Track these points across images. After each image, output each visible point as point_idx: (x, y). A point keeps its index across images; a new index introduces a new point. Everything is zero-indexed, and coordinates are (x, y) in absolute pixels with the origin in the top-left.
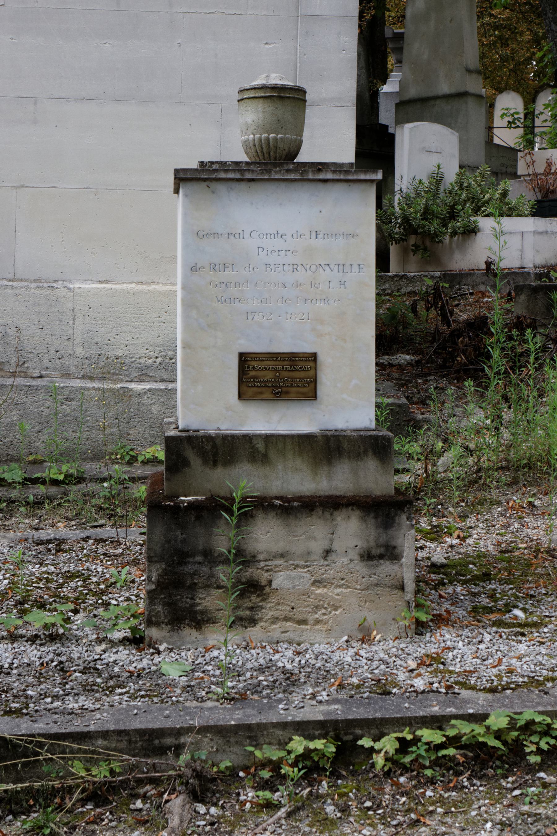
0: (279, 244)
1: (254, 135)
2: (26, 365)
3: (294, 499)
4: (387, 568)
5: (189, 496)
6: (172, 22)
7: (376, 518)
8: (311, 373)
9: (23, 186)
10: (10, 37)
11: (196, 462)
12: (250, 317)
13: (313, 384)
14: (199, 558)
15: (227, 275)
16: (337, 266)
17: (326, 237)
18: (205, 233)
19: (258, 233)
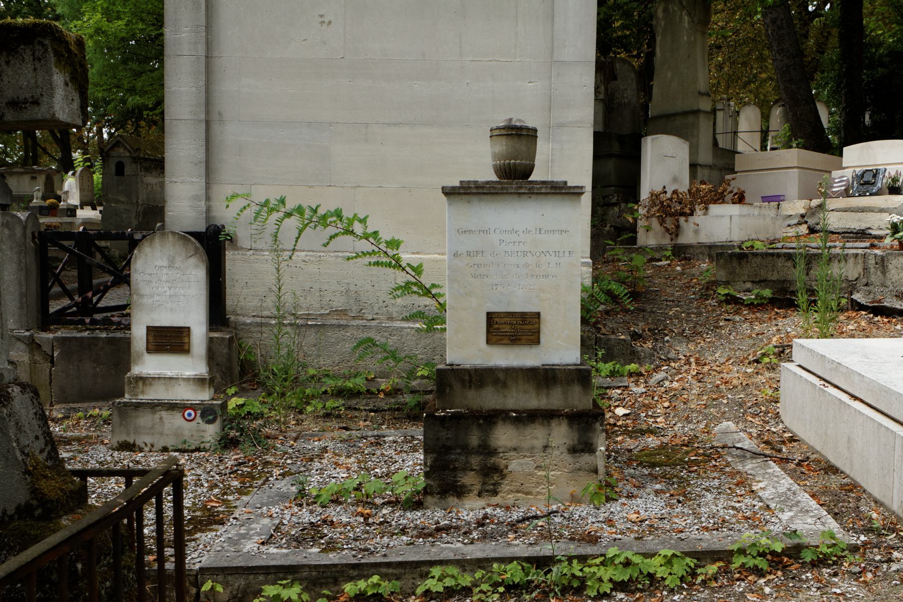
3: (524, 412)
4: (586, 458)
7: (579, 424)
8: (536, 326)
11: (457, 386)
14: (458, 451)
15: (478, 259)
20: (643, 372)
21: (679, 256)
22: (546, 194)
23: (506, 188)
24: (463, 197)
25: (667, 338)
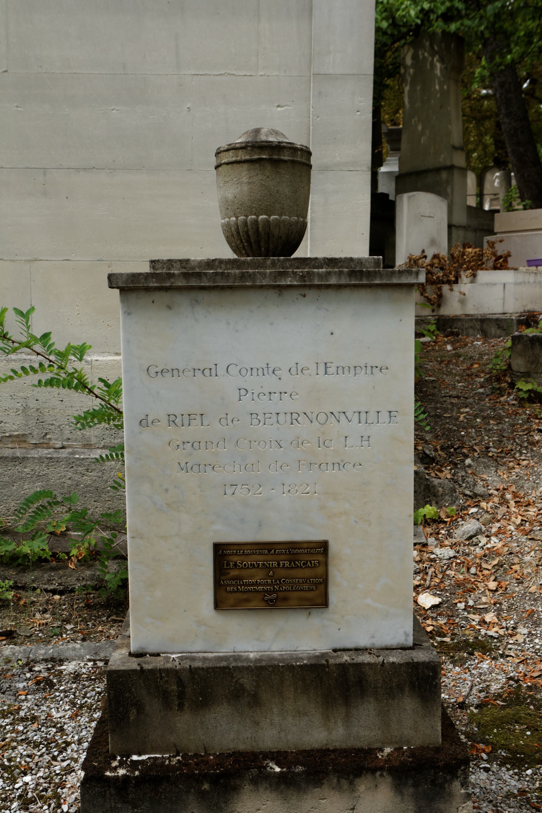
0: (269, 382)
1: (237, 218)
2: (48, 437)
5: (145, 754)
6: (181, 85)
7: (416, 785)
8: (320, 570)
9: (36, 260)
10: (16, 104)
11: (153, 706)
12: (229, 491)
13: (322, 587)
16: (357, 415)
17: (340, 371)
18: (159, 369)
19: (239, 368)
20: (443, 516)
21: (444, 330)
22: (339, 287)
23: (252, 276)
24: (157, 296)
25: (468, 461)
